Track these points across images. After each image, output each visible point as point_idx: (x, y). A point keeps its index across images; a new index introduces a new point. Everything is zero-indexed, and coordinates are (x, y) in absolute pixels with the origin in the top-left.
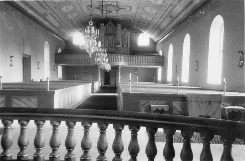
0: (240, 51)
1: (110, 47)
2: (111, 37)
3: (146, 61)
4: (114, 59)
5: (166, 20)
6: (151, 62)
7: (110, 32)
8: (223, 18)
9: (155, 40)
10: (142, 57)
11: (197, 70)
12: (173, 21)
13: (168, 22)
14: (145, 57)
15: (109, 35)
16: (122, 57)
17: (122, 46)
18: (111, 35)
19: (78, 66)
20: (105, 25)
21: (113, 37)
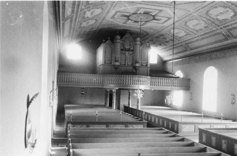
0: (233, 94)
1: (127, 65)
2: (128, 53)
3: (173, 84)
4: (154, 83)
5: (180, 48)
6: (177, 86)
7: (127, 47)
8: (213, 66)
9: (166, 59)
10: (125, 76)
11: (191, 99)
12: (186, 51)
13: (181, 50)
14: (130, 76)
15: (126, 50)
16: (144, 79)
17: (142, 65)
18: (129, 50)
19: (165, 90)
20: (121, 38)
21: (131, 53)
